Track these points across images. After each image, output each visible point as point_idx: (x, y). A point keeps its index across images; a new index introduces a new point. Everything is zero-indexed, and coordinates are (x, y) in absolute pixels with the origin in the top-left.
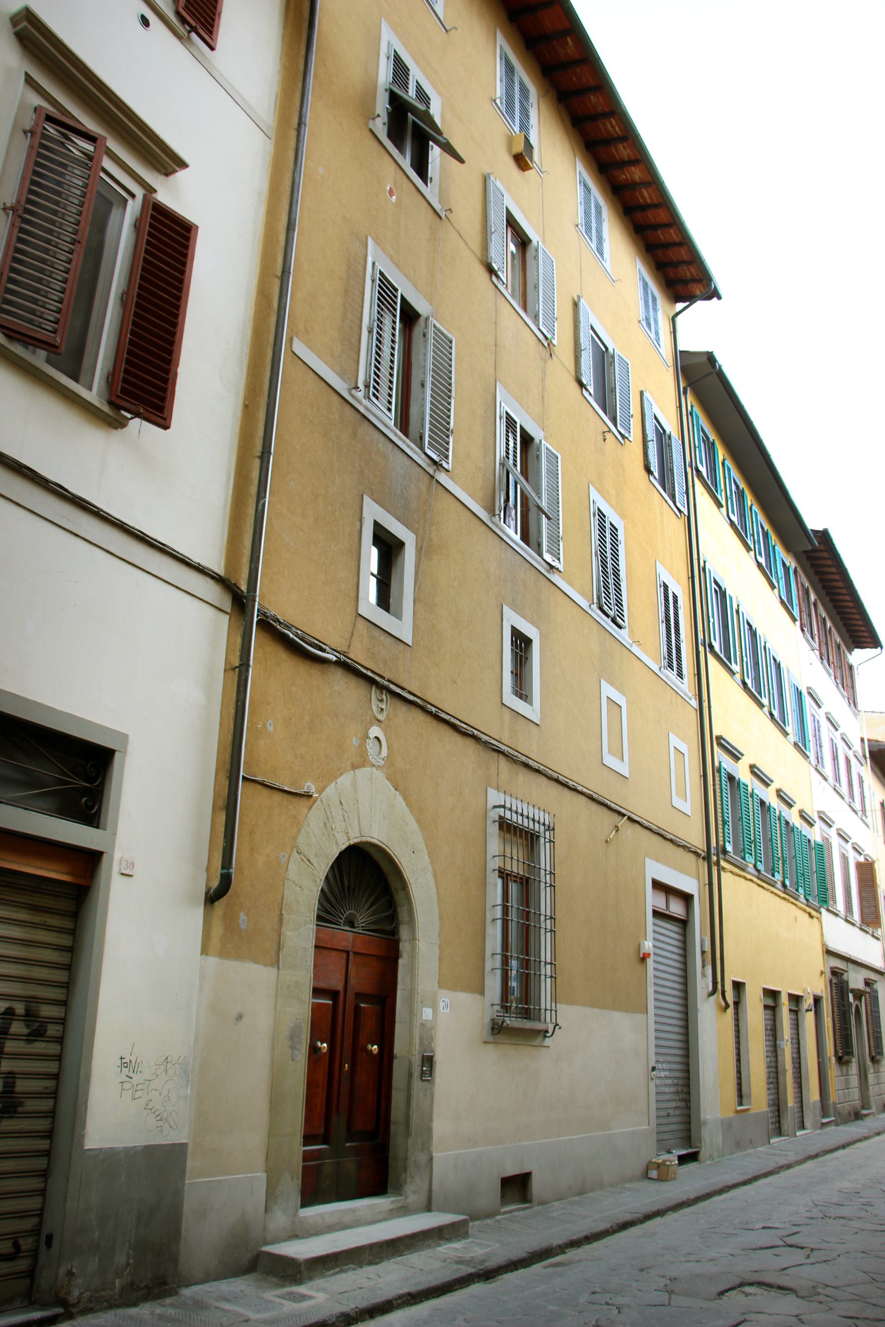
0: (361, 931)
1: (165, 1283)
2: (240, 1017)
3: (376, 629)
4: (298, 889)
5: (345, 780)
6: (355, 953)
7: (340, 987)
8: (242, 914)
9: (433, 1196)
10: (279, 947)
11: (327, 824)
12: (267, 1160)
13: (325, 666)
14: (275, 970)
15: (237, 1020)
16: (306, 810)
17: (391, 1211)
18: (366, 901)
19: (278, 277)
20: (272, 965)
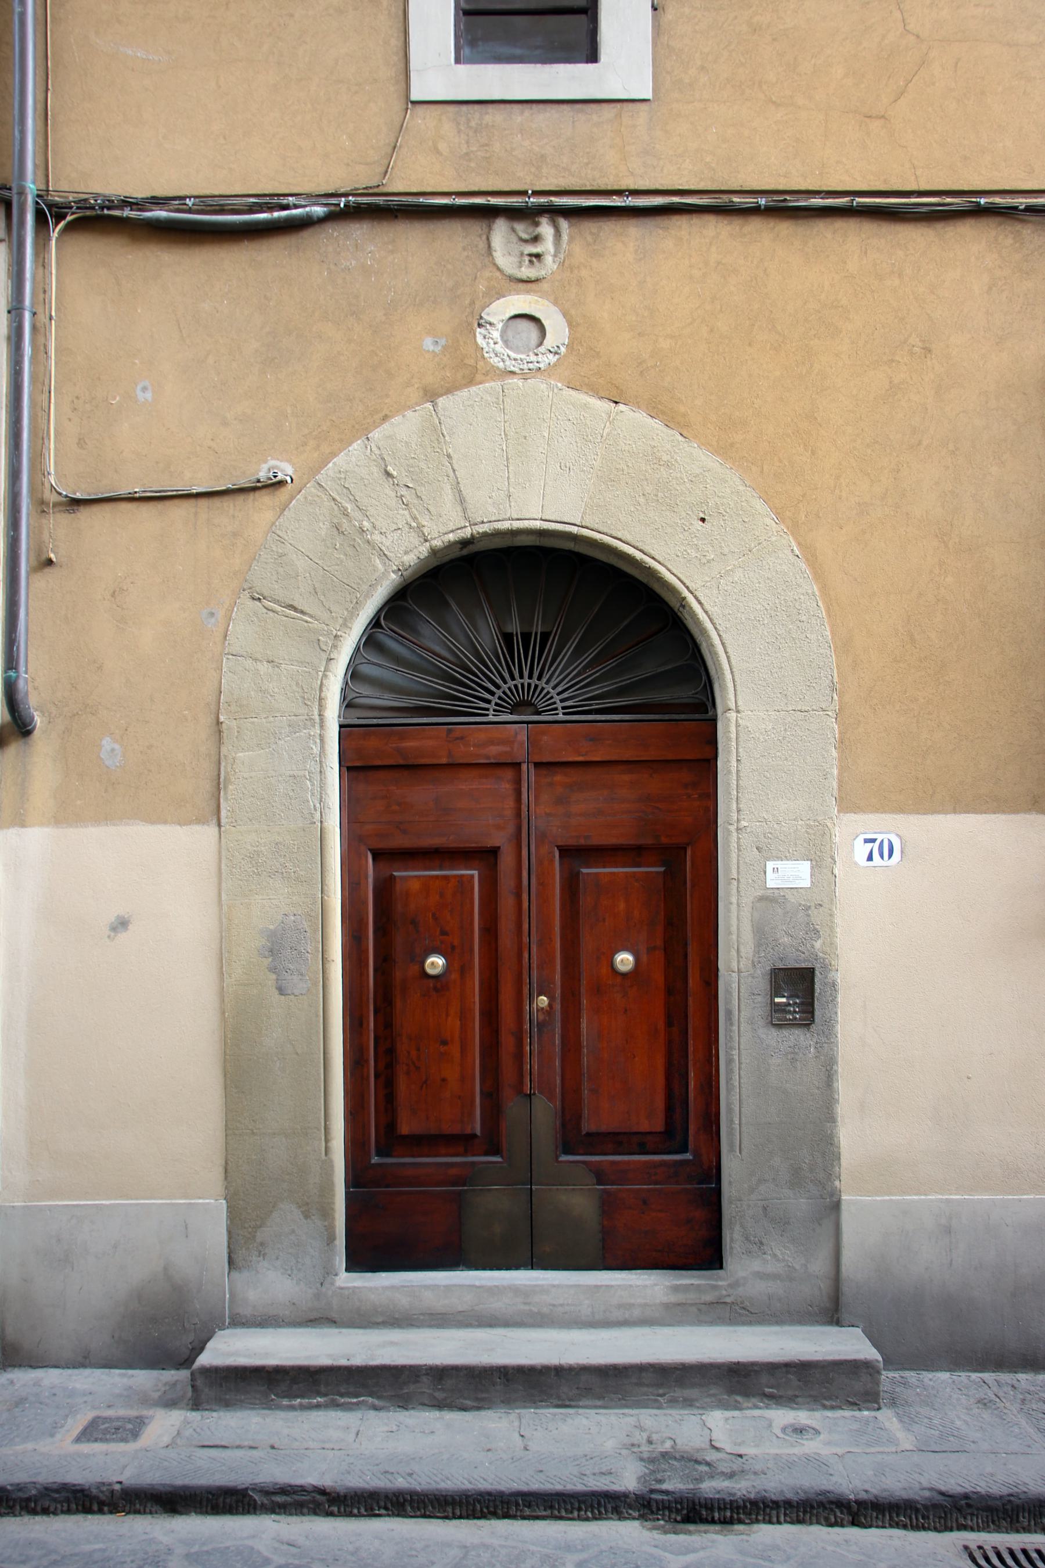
0: (561, 717)
1: (788, 1223)
2: (122, 924)
3: (490, 108)
4: (264, 668)
5: (405, 428)
6: (537, 765)
7: (499, 839)
8: (107, 743)
9: (843, 1299)
10: (218, 786)
11: (345, 525)
12: (226, 1178)
13: (306, 234)
14: (211, 830)
15: (114, 929)
16: (269, 515)
17: (667, 1306)
18: (590, 665)
19: (619, 116)
20: (200, 821)
